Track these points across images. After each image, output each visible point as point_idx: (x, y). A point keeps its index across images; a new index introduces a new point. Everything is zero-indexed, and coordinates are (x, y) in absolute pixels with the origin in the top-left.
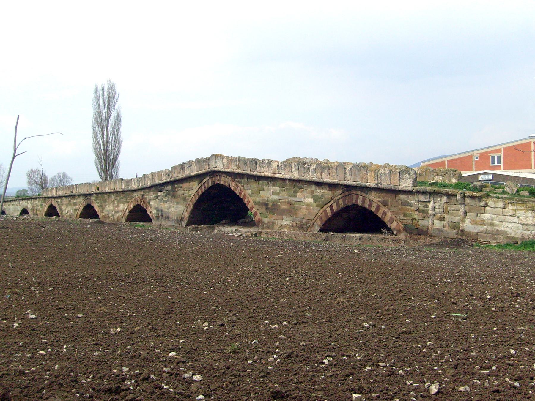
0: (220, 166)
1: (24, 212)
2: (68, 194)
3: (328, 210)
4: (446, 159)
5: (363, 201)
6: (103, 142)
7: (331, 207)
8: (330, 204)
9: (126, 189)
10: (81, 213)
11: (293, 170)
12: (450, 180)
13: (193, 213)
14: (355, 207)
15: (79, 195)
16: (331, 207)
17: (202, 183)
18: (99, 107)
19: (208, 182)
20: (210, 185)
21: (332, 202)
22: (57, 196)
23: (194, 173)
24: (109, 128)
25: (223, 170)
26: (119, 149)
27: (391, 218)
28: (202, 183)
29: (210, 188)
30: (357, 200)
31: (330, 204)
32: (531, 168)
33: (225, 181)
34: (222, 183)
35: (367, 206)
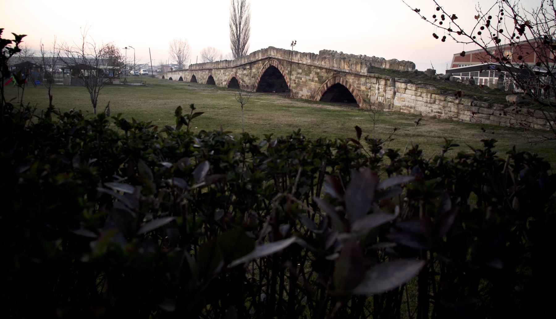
0: (273, 54)
1: (181, 79)
2: (201, 69)
3: (325, 86)
4: (471, 53)
5: (343, 82)
6: (237, 34)
7: (327, 84)
8: (326, 82)
9: (228, 67)
10: (207, 81)
11: (308, 58)
12: (408, 69)
13: (260, 83)
14: (339, 84)
15: (206, 69)
16: (327, 84)
17: (264, 65)
18: (235, 11)
19: (267, 64)
20: (268, 66)
21: (327, 81)
22: (236, 68)
23: (260, 59)
24: (241, 26)
25: (274, 57)
26: (247, 40)
27: (357, 93)
28: (264, 65)
29: (268, 68)
30: (340, 81)
31: (326, 82)
32: (469, 61)
33: (275, 64)
34: (274, 65)
35: (344, 84)
